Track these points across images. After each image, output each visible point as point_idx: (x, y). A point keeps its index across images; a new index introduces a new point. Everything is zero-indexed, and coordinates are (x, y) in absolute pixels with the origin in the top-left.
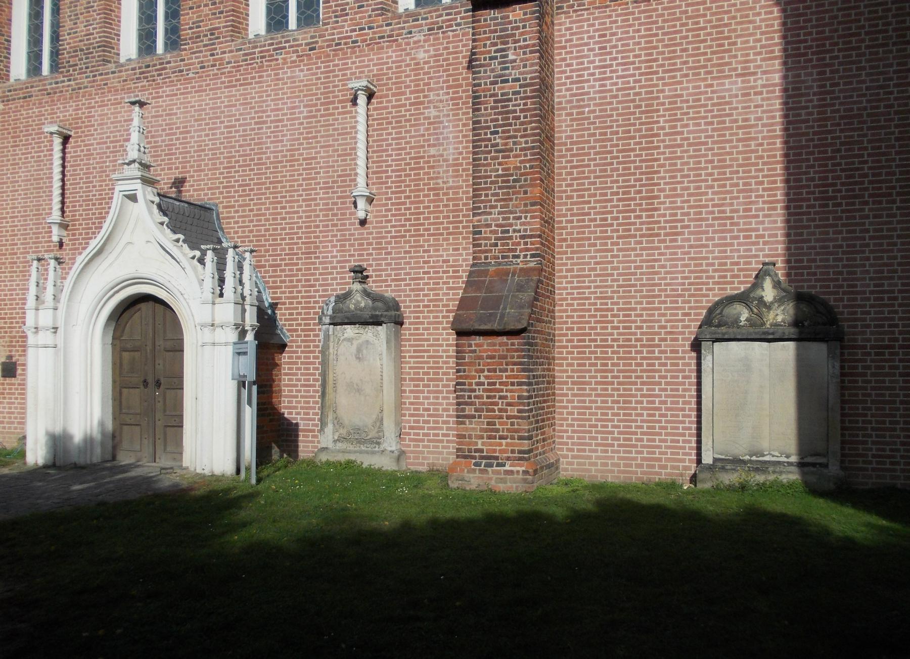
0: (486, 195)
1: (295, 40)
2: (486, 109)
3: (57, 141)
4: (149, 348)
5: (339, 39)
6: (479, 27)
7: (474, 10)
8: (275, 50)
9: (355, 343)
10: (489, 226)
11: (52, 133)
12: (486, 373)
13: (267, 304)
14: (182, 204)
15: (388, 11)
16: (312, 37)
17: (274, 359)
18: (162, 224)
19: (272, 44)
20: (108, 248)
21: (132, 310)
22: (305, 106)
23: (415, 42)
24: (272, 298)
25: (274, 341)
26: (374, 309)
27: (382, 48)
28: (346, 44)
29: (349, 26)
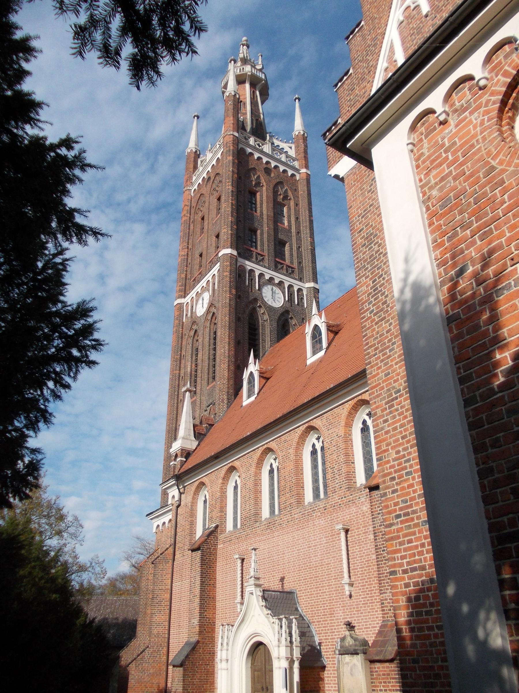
0: (384, 583)
1: (319, 506)
2: (379, 539)
3: (239, 562)
4: (264, 669)
5: (334, 503)
6: (373, 499)
7: (370, 492)
8: (312, 511)
9: (350, 665)
10: (386, 599)
11: (237, 558)
12: (383, 684)
13: (317, 644)
14: (276, 593)
15: (352, 488)
16: (325, 504)
17: (319, 675)
18: (263, 606)
19: (311, 509)
20: (246, 619)
21: (258, 649)
22: (325, 538)
23: (362, 502)
24: (319, 640)
25: (319, 664)
26: (356, 645)
27: (350, 506)
28: (337, 506)
29: (337, 497)
